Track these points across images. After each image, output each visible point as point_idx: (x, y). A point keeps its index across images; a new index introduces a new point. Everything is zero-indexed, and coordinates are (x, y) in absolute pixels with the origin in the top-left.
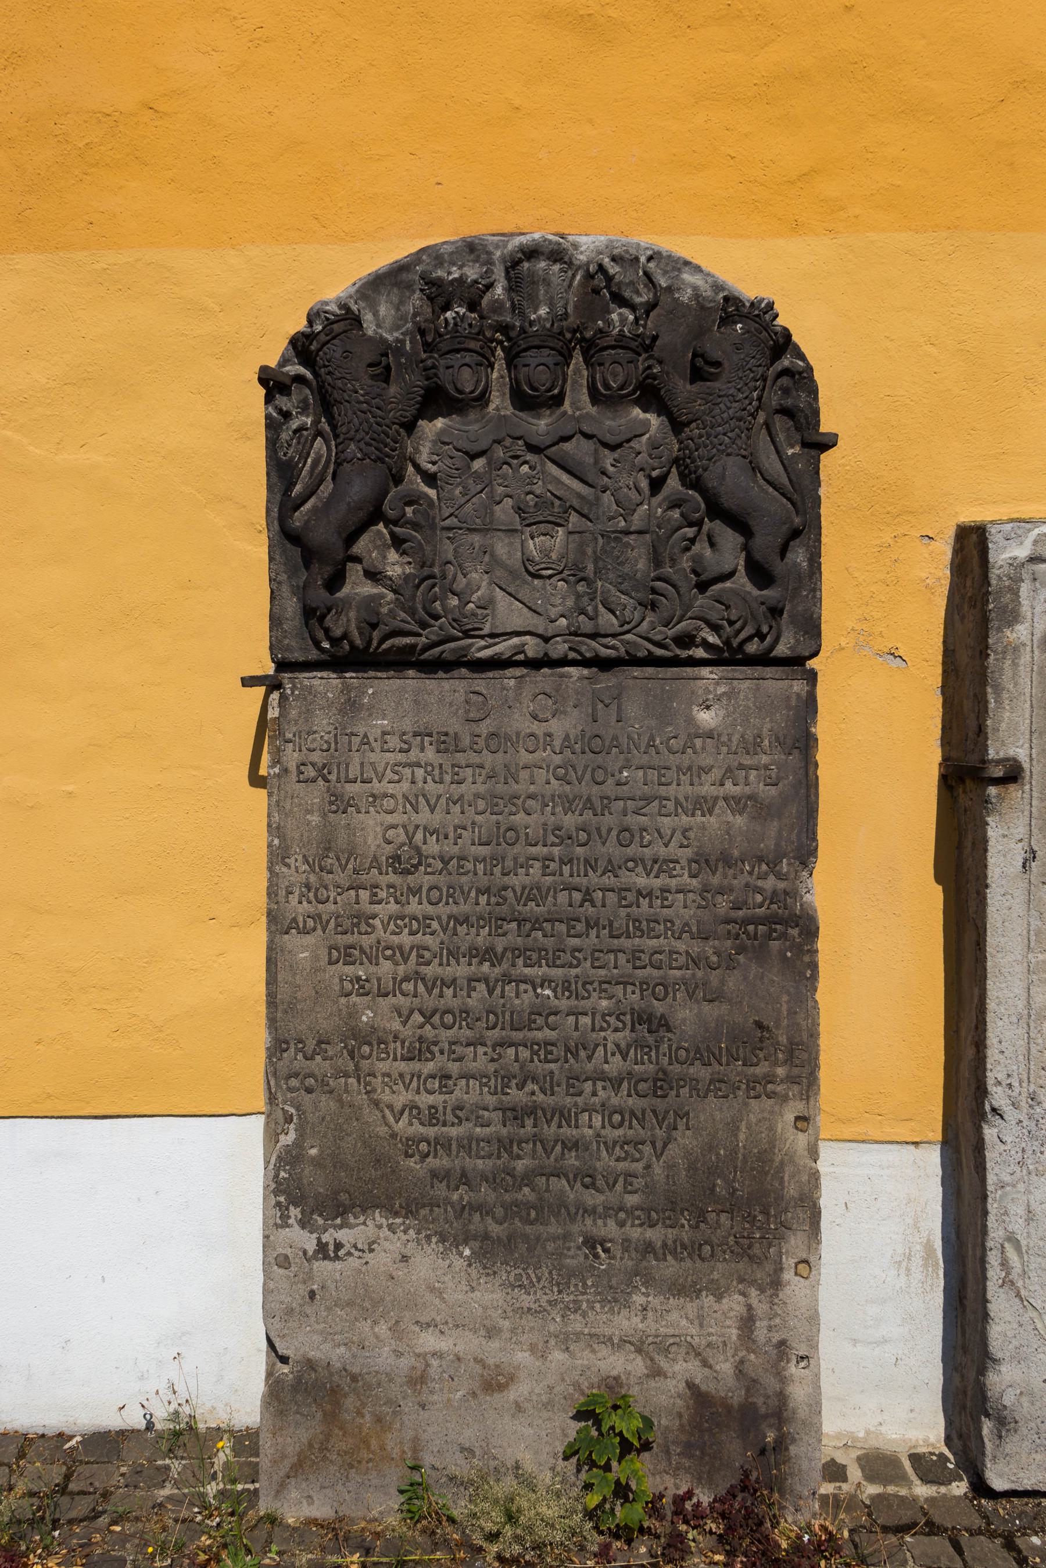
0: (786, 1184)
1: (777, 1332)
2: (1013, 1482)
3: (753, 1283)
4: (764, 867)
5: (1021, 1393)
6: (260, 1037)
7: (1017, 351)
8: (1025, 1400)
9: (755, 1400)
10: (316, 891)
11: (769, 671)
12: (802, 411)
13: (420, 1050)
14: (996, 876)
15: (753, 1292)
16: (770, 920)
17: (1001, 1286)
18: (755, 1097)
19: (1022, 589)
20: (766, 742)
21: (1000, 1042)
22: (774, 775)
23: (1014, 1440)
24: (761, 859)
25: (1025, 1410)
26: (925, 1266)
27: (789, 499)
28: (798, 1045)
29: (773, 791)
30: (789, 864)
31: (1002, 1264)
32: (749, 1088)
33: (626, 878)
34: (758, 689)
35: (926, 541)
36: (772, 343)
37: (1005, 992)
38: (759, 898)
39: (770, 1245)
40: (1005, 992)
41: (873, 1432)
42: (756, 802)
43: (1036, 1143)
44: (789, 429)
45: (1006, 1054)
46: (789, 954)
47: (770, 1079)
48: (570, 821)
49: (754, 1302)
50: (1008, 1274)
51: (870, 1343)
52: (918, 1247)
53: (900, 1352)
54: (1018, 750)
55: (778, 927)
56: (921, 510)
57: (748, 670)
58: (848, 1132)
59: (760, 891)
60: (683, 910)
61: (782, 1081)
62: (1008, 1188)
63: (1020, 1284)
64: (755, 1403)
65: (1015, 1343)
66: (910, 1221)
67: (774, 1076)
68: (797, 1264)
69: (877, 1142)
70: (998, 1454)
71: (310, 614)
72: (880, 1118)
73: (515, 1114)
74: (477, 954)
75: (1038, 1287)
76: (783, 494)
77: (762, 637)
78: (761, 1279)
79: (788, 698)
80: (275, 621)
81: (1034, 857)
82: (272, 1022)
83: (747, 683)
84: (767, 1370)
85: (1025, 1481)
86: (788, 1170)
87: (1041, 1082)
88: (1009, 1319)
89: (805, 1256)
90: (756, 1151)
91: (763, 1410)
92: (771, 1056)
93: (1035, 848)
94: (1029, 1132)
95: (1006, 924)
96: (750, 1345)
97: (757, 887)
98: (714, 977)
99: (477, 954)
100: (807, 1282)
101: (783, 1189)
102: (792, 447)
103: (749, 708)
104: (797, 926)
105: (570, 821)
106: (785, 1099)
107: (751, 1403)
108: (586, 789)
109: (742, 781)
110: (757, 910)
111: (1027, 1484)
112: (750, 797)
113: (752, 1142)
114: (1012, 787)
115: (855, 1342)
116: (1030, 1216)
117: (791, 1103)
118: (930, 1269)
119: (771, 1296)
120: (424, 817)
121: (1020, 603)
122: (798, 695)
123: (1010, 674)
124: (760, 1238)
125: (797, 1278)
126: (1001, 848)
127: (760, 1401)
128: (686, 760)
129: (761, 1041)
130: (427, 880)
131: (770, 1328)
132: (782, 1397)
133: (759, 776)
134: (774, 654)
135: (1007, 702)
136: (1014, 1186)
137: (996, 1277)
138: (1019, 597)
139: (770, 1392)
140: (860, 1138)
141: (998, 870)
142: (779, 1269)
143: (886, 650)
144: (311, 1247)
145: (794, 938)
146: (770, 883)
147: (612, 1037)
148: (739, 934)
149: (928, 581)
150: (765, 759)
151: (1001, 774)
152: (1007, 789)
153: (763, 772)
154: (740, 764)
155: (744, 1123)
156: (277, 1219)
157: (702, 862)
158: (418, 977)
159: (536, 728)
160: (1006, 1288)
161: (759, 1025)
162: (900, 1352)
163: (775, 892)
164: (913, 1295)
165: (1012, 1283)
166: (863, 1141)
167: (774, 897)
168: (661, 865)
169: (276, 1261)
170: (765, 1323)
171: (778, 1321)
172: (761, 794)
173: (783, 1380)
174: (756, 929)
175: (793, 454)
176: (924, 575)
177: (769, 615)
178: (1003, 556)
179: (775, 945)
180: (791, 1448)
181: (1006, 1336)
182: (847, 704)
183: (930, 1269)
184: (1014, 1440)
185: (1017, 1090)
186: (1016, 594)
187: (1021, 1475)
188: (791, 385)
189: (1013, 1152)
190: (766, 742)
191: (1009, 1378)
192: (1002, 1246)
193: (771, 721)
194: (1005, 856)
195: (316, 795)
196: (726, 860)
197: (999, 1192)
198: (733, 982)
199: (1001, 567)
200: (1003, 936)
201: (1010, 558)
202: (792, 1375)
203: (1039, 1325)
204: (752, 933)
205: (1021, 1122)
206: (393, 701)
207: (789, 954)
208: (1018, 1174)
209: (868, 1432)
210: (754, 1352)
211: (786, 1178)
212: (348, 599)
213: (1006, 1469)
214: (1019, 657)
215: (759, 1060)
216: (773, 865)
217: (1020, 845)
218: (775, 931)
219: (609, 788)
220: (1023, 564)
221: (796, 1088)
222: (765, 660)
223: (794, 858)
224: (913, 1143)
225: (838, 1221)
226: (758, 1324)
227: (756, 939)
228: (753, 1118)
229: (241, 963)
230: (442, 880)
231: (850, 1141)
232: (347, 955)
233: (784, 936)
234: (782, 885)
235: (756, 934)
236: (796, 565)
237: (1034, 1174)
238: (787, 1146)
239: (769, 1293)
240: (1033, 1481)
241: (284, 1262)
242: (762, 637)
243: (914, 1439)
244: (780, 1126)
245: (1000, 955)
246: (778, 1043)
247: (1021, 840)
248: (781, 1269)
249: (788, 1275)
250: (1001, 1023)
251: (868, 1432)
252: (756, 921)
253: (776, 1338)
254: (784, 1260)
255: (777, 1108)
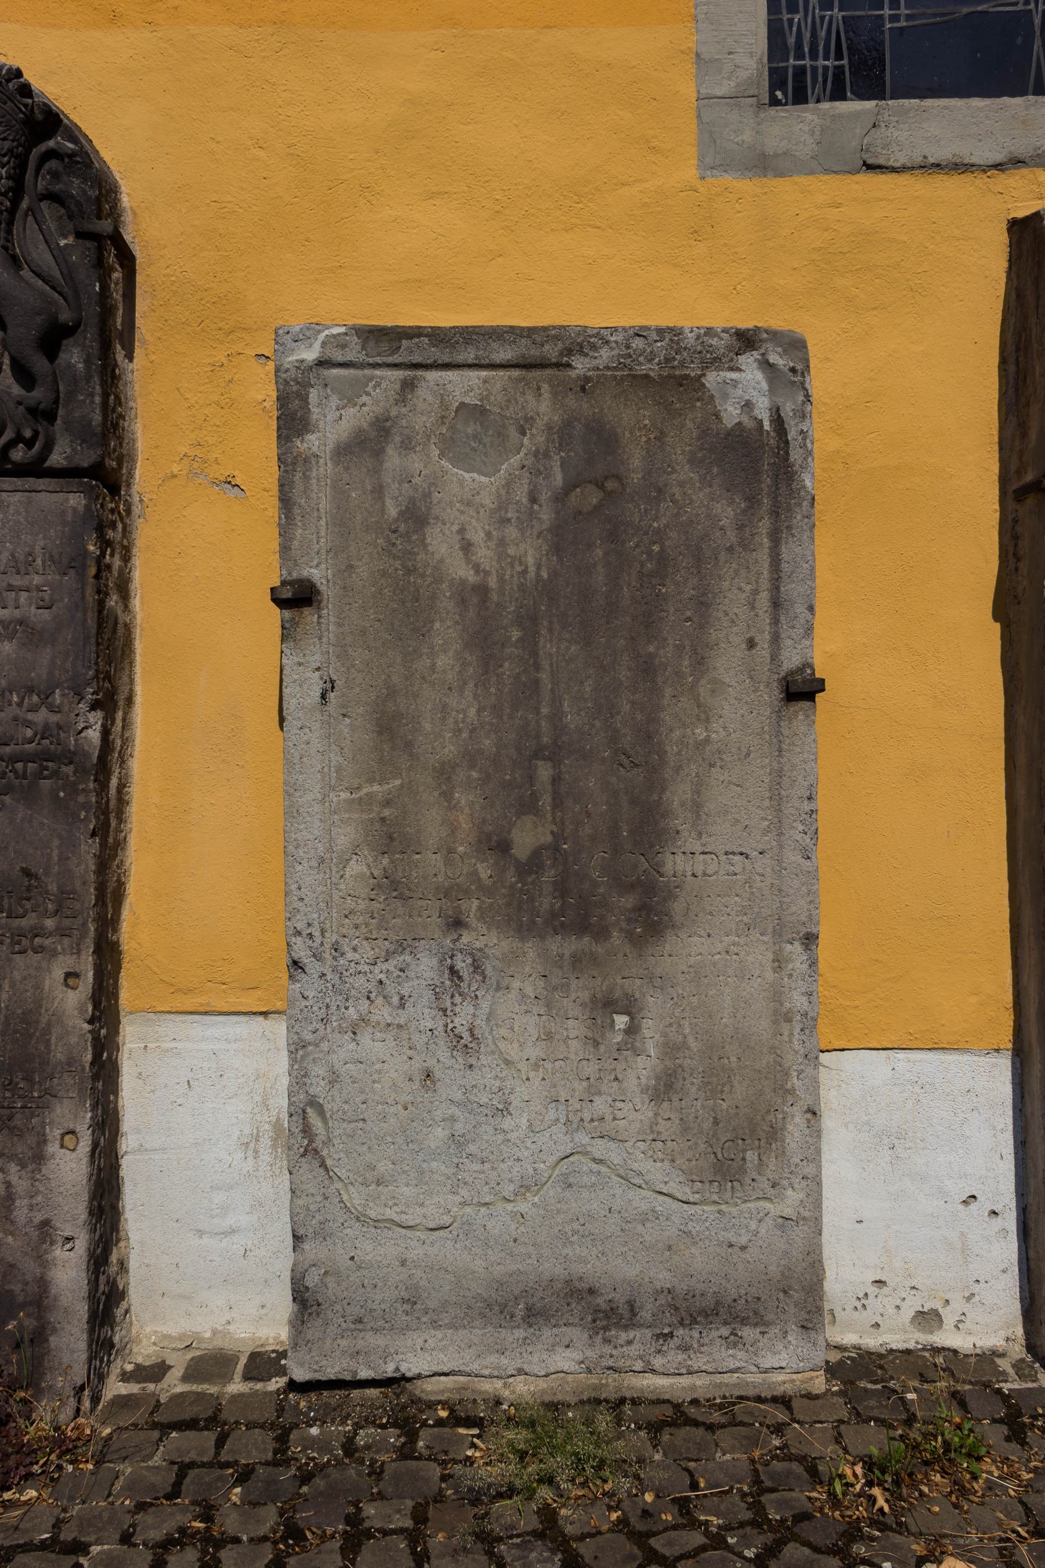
0: (53, 1047)
1: (39, 1211)
2: (316, 1371)
3: (12, 1157)
4: (35, 698)
5: (326, 1273)
7: (351, 157)
8: (330, 1281)
9: (12, 1287)
11: (42, 483)
12: (72, 197)
14: (292, 708)
15: (13, 1168)
16: (42, 757)
17: (303, 1155)
18: (20, 953)
19: (311, 395)
20: (39, 561)
21: (300, 889)
22: (47, 598)
23: (316, 1324)
24: (31, 690)
25: (330, 1291)
26: (274, 1147)
27: (60, 293)
28: (69, 893)
29: (46, 615)
30: (63, 695)
31: (304, 1131)
32: (14, 943)
34: (30, 502)
35: (263, 360)
36: (22, 116)
37: (305, 833)
38: (29, 733)
39: (32, 1116)
40: (305, 833)
41: (221, 1332)
42: (27, 626)
43: (340, 998)
44: (60, 217)
45: (305, 902)
46: (62, 794)
47: (37, 932)
49: (14, 1179)
50: (311, 1141)
51: (216, 1234)
52: (267, 1127)
53: (250, 1243)
54: (312, 570)
55: (50, 764)
56: (255, 327)
57: (18, 482)
58: (189, 1003)
59: (28, 724)
61: (51, 934)
62: (310, 1048)
63: (324, 1153)
64: (12, 1291)
65: (319, 1217)
66: (258, 1098)
67: (41, 928)
68: (63, 1135)
69: (221, 1014)
70: (300, 1341)
72: (224, 987)
75: (342, 1155)
76: (53, 288)
77: (30, 444)
78: (23, 1153)
79: (63, 513)
81: (333, 687)
83: (18, 496)
84: (26, 1254)
85: (328, 1370)
86: (56, 1032)
87: (344, 931)
88: (312, 1191)
89: (71, 1126)
90: (20, 1011)
91: (21, 1299)
92: (38, 906)
93: (334, 677)
94: (333, 986)
95: (305, 759)
96: (8, 1226)
97: (26, 720)
100: (74, 1155)
101: (49, 1053)
102: (65, 238)
103: (20, 522)
104: (71, 763)
106: (54, 954)
107: (7, 1291)
109: (11, 603)
110: (27, 746)
111: (331, 1373)
112: (21, 622)
113: (16, 1002)
114: (306, 611)
115: (200, 1233)
116: (334, 1079)
117: (61, 958)
118: (279, 1150)
119: (33, 1172)
121: (309, 409)
122: (74, 509)
123: (302, 488)
124: (22, 1108)
125: (63, 1150)
126: (296, 677)
127: (17, 1288)
129: (29, 889)
131: (31, 1208)
132: (43, 1283)
133: (30, 598)
134: (48, 464)
135: (299, 518)
136: (317, 1045)
137: (297, 1145)
138: (309, 403)
139: (29, 1278)
140: (202, 1009)
141: (294, 701)
142: (43, 1141)
143: (223, 479)
145: (68, 776)
146: (42, 716)
148: (5, 773)
149: (265, 404)
150: (37, 580)
151: (289, 595)
152: (302, 613)
153: (35, 593)
154: (9, 585)
155: (7, 981)
160: (309, 1157)
161: (27, 873)
162: (250, 1243)
163: (47, 726)
164: (262, 1179)
165: (316, 1151)
166: (206, 1013)
167: (45, 732)
170: (26, 1201)
171: (39, 1198)
172: (33, 619)
173: (44, 1263)
174: (25, 767)
175: (66, 245)
176: (260, 397)
177: (29, 417)
178: (290, 359)
179: (46, 784)
180: (51, 1339)
181: (308, 1209)
182: (182, 537)
183: (279, 1150)
184: (316, 1324)
185: (318, 940)
186: (305, 399)
187: (324, 1363)
188: (61, 169)
189: (315, 1008)
190: (39, 561)
191: (312, 1257)
192: (304, 1111)
193: (45, 538)
194: (300, 686)
197: (301, 1052)
199: (287, 370)
200: (302, 773)
201: (297, 361)
202: (55, 1258)
203: (345, 1197)
204: (21, 772)
205: (324, 975)
207: (62, 794)
208: (321, 1032)
209: (214, 1332)
210: (12, 1234)
211: (53, 1040)
213: (308, 1357)
214: (311, 469)
215: (26, 912)
216: (46, 696)
217: (317, 674)
218: (46, 768)
220: (311, 368)
221: (66, 941)
222: (36, 469)
223: (68, 688)
224: (261, 1013)
225: (179, 1101)
226: (18, 1203)
227: (25, 778)
228: (17, 975)
231: (191, 1013)
233: (55, 774)
234: (54, 718)
235: (25, 771)
236: (70, 366)
237: (336, 1031)
238: (55, 1005)
239: (30, 1168)
240: (337, 1369)
242: (30, 444)
243: (264, 1337)
244: (47, 983)
245: (297, 794)
246: (47, 892)
247: (318, 669)
248: (45, 1142)
249: (53, 1147)
250: (300, 867)
251: (214, 1332)
252: (26, 758)
253: (38, 1218)
254: (48, 1131)
255: (44, 964)
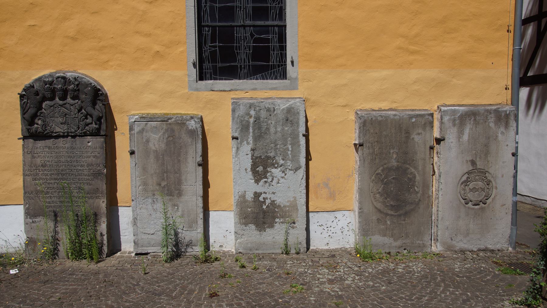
6: (23, 191)
10: (30, 170)
13: (47, 193)
33: (77, 168)
48: (69, 159)
60: (86, 172)
71: (28, 130)
73: (61, 202)
74: (55, 179)
80: (22, 130)
82: (24, 189)
98: (91, 182)
99: (55, 179)
105: (69, 159)
108: (71, 155)
120: (46, 159)
128: (86, 150)
130: (47, 168)
144: (31, 221)
147: (75, 191)
156: (26, 217)
157: (88, 165)
158: (46, 182)
159: (64, 146)
167: (99, 170)
168: (82, 166)
169: (26, 224)
195: (30, 156)
196: (92, 165)
198: (93, 182)
206: (41, 144)
212: (34, 131)
219: (74, 155)
229: (19, 182)
230: (49, 168)
232: (35, 179)
241: (27, 224)
